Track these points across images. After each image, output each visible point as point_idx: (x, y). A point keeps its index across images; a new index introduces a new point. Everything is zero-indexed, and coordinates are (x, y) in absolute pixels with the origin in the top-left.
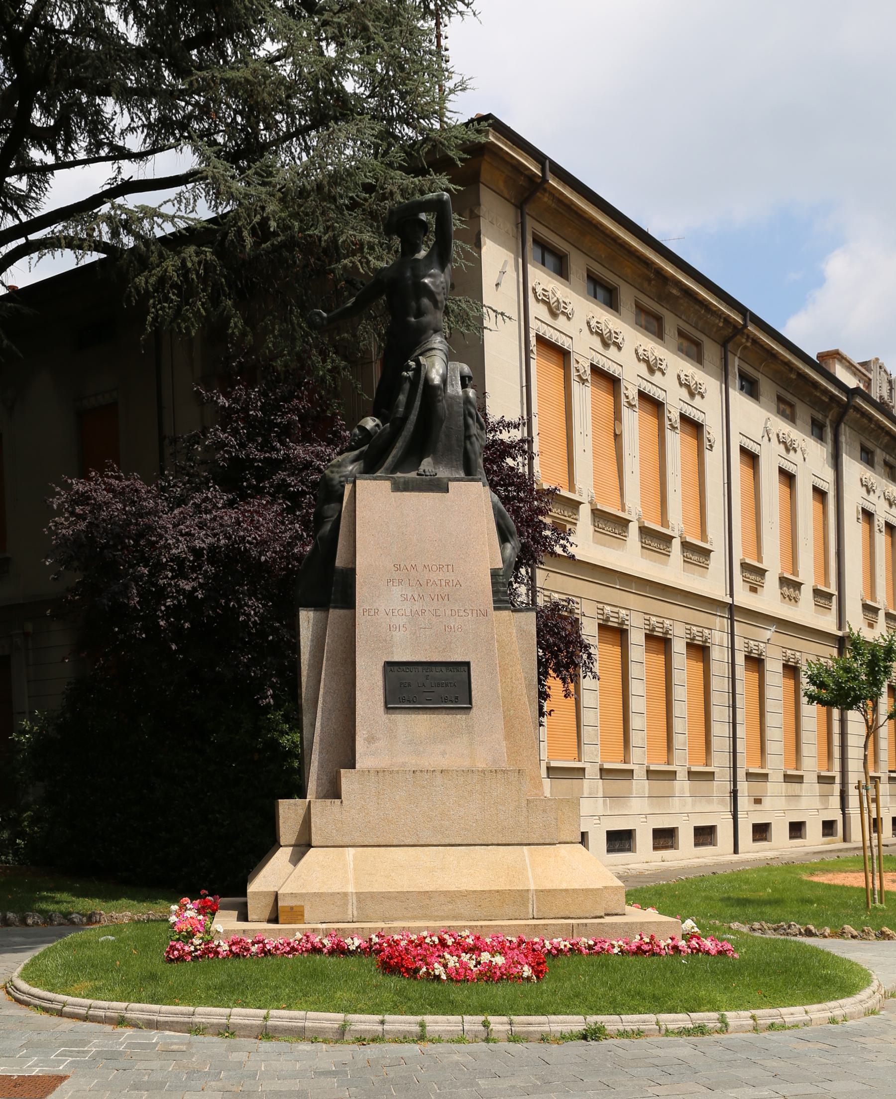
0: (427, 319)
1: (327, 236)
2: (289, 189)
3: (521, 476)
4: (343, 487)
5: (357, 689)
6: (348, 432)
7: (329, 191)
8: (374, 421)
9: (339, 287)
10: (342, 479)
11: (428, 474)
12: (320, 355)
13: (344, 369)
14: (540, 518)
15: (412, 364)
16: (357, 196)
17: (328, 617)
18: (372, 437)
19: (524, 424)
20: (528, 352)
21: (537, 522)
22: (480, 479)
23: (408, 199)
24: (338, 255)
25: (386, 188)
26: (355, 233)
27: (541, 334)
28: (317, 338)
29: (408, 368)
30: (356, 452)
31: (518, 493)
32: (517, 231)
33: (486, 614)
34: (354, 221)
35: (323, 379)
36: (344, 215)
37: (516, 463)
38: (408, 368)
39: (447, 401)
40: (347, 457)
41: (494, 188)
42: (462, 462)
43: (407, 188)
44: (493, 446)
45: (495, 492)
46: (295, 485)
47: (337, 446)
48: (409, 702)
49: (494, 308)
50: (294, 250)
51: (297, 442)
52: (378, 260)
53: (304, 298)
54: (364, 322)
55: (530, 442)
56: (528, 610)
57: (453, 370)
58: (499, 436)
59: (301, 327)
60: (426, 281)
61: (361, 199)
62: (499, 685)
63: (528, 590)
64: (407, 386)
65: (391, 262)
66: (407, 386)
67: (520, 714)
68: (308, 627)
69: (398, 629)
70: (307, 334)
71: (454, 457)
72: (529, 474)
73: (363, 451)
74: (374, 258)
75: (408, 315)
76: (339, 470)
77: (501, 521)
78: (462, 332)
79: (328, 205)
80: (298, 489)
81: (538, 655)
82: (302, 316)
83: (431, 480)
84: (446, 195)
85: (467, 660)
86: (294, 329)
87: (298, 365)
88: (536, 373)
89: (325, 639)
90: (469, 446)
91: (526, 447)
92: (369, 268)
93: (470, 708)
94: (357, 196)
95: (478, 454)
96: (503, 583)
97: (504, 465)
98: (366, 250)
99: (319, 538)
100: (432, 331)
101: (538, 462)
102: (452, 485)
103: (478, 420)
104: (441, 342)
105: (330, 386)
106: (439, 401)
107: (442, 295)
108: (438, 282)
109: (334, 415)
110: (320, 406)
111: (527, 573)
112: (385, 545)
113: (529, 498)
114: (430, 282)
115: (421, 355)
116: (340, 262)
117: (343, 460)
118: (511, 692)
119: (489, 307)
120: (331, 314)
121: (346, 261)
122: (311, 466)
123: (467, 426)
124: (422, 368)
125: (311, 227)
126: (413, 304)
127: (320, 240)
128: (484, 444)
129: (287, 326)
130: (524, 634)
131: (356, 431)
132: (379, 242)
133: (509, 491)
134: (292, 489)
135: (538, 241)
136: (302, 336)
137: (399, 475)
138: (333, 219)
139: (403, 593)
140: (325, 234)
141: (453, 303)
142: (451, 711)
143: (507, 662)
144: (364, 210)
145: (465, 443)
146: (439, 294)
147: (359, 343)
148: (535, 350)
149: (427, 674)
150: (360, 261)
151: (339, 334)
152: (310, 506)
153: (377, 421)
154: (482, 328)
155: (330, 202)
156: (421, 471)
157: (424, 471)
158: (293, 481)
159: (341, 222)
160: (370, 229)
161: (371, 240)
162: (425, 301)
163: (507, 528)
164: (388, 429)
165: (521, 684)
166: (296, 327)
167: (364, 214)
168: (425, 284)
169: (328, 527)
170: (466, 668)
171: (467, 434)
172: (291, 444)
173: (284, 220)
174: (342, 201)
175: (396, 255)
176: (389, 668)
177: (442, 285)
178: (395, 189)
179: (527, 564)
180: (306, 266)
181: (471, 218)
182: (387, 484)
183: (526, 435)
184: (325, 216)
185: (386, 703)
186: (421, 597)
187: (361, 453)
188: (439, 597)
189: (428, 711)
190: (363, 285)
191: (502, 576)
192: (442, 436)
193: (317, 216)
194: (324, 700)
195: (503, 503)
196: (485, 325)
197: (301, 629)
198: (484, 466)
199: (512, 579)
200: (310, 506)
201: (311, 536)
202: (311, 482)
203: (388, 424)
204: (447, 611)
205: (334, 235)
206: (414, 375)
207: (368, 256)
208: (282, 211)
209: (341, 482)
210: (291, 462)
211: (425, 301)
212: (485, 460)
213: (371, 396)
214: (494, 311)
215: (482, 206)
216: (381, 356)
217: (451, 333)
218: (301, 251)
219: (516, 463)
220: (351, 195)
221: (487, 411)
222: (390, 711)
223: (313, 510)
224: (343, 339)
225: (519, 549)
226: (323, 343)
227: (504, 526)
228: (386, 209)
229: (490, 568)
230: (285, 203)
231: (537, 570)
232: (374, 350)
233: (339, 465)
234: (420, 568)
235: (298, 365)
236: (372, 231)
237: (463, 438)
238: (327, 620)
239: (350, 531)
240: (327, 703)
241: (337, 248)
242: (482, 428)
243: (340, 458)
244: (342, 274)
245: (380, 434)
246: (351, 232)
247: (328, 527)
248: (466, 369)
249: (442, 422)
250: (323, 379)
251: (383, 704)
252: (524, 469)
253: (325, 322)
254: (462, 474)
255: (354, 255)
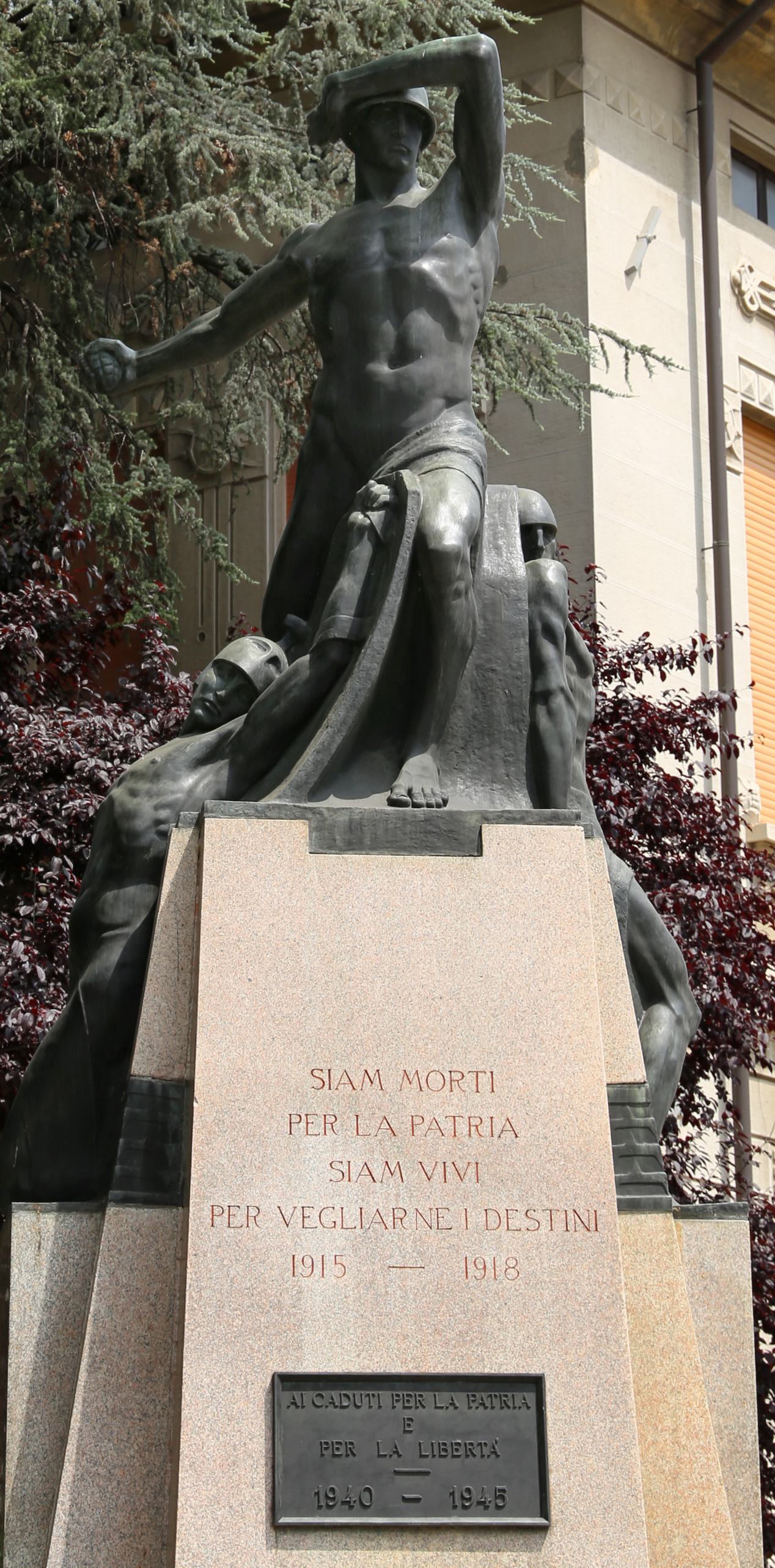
0: (419, 370)
1: (145, 139)
2: (41, 17)
3: (701, 805)
4: (165, 836)
5: (184, 1463)
6: (184, 677)
7: (156, 22)
8: (265, 647)
9: (173, 275)
10: (163, 814)
11: (420, 800)
12: (112, 457)
13: (180, 496)
14: (760, 927)
15: (382, 491)
16: (235, 36)
17: (99, 1230)
18: (257, 693)
19: (708, 655)
20: (718, 452)
21: (748, 941)
22: (578, 817)
23: (377, 46)
24: (174, 190)
25: (318, 19)
26: (224, 132)
27: (756, 404)
28: (105, 411)
29: (368, 503)
30: (210, 737)
31: (691, 855)
32: (687, 130)
33: (593, 1226)
34: (224, 101)
35: (116, 526)
36: (193, 85)
37: (684, 766)
38: (368, 503)
39: (480, 594)
40: (178, 750)
41: (622, 18)
42: (524, 768)
43: (377, 19)
44: (615, 717)
45: (621, 854)
46: (19, 828)
47: (149, 714)
48: (349, 1506)
49: (621, 336)
50: (49, 175)
51: (32, 701)
52: (289, 205)
53: (73, 301)
54: (243, 368)
55: (727, 706)
56: (728, 1211)
57: (501, 507)
58: (633, 690)
59: (59, 383)
60: (427, 265)
61: (246, 45)
62: (636, 1451)
63: (725, 1145)
64: (363, 551)
65: (327, 214)
66: (363, 551)
67: (705, 1550)
68: (38, 1264)
69: (318, 1271)
70: (76, 402)
71: (499, 752)
72: (725, 799)
73: (230, 732)
74: (278, 200)
75: (372, 357)
76: (155, 788)
77: (640, 941)
78: (526, 400)
79: (153, 60)
80: (27, 840)
81: (759, 1354)
82: (63, 353)
83: (427, 820)
84: (486, 44)
85: (534, 1370)
86: (38, 388)
87: (46, 485)
88: (743, 511)
89: (87, 1301)
90: (544, 721)
91: (714, 722)
92: (263, 227)
93: (544, 1529)
94: (235, 36)
95: (571, 744)
96: (647, 1128)
97: (650, 771)
98: (254, 178)
99: (85, 988)
100: (440, 402)
101: (752, 764)
102: (491, 833)
103: (572, 648)
104: (465, 431)
105: (137, 544)
106: (458, 594)
107: (472, 304)
108: (460, 270)
109: (146, 624)
110: (107, 600)
111: (722, 1093)
112: (286, 1011)
113: (727, 870)
114: (436, 268)
115: (405, 465)
116: (179, 209)
117: (169, 758)
118: (675, 1476)
119: (605, 333)
120: (150, 351)
121: (197, 207)
122: (71, 771)
123: (538, 665)
124: (410, 503)
125: (101, 114)
126: (388, 328)
127: (124, 151)
128: (589, 715)
129: (19, 378)
130: (713, 1288)
131: (210, 675)
132: (295, 158)
133: (664, 849)
134: (9, 838)
135: (742, 157)
136: (61, 406)
137: (333, 802)
138: (164, 94)
139: (338, 1156)
140: (140, 134)
141: (502, 321)
142: (484, 1540)
143: (660, 1377)
144: (252, 73)
145: (533, 714)
146: (462, 301)
147: (226, 427)
148: (739, 446)
149: (408, 1414)
150: (237, 207)
151: (168, 400)
152: (61, 887)
153: (275, 648)
154: (583, 388)
155: (157, 52)
156: (400, 792)
157: (410, 792)
158: (14, 814)
159: (184, 104)
160: (268, 124)
161: (272, 151)
162: (422, 322)
163: (659, 959)
164: (306, 673)
165: (705, 1449)
166: (46, 381)
167: (252, 84)
168: (422, 276)
169: (111, 957)
170: (531, 1397)
171: (539, 687)
172: (14, 708)
173: (24, 95)
174: (190, 50)
175: (342, 191)
176: (285, 1397)
177: (472, 278)
178: (342, 20)
179: (721, 1066)
180: (83, 218)
181: (556, 96)
182: (299, 830)
183: (714, 686)
184: (141, 86)
185: (274, 1511)
186: (394, 1170)
187: (224, 738)
188: (450, 1169)
189: (409, 1538)
190: (246, 270)
191: (645, 1105)
192: (465, 692)
193: (119, 87)
194: (74, 1503)
195: (646, 885)
196: (594, 381)
197: (14, 1271)
198: (590, 782)
199: (676, 1112)
200: (61, 887)
201: (61, 977)
202: (68, 816)
203: (307, 657)
204: (472, 1214)
205: (165, 138)
206: (387, 523)
207: (260, 194)
208: (19, 72)
209: (158, 822)
210: (10, 759)
211: (422, 322)
212: (593, 759)
213: (258, 574)
214: (622, 343)
215: (588, 67)
216: (289, 462)
217: (495, 402)
218: (69, 176)
219: (684, 766)
220: (216, 33)
221: (599, 619)
222: (288, 1538)
223: (72, 902)
224: (181, 416)
225: (696, 1023)
226: (122, 427)
227: (648, 955)
228: (315, 72)
229: (606, 1080)
230: (29, 52)
231: (752, 1083)
232: (269, 444)
233: (155, 774)
234: (392, 1080)
235: (46, 485)
236: (274, 129)
237: (526, 698)
238: (97, 1240)
239: (180, 969)
240: (82, 1512)
241: (171, 172)
242: (583, 669)
243: (159, 753)
244: (185, 242)
245: (281, 685)
246: (214, 131)
247: (111, 957)
248: (539, 507)
249: (465, 651)
250: (116, 526)
251: (263, 1514)
252: (708, 786)
253: (130, 373)
254: (523, 802)
255: (220, 188)
